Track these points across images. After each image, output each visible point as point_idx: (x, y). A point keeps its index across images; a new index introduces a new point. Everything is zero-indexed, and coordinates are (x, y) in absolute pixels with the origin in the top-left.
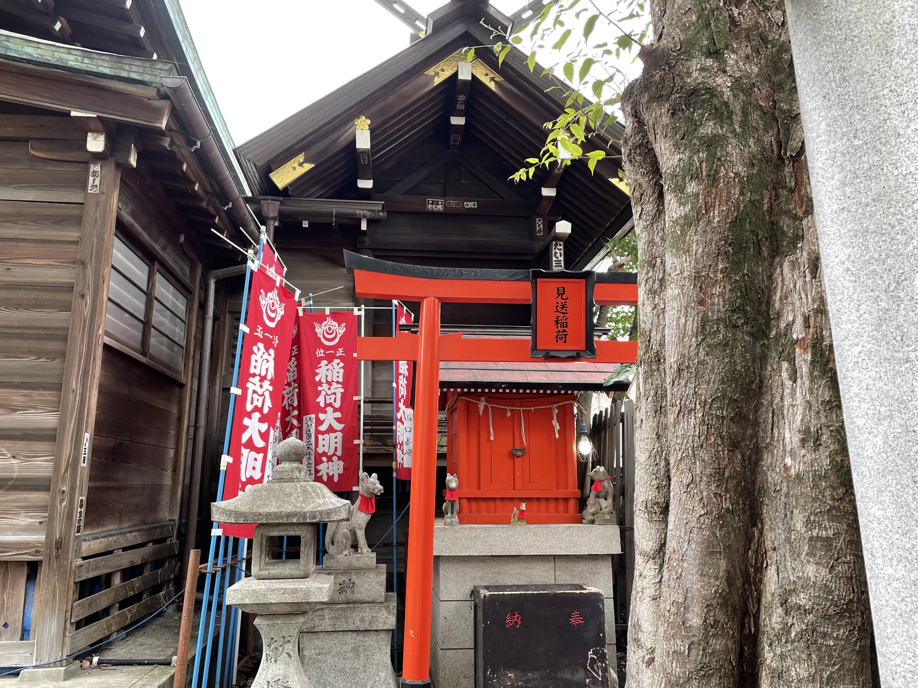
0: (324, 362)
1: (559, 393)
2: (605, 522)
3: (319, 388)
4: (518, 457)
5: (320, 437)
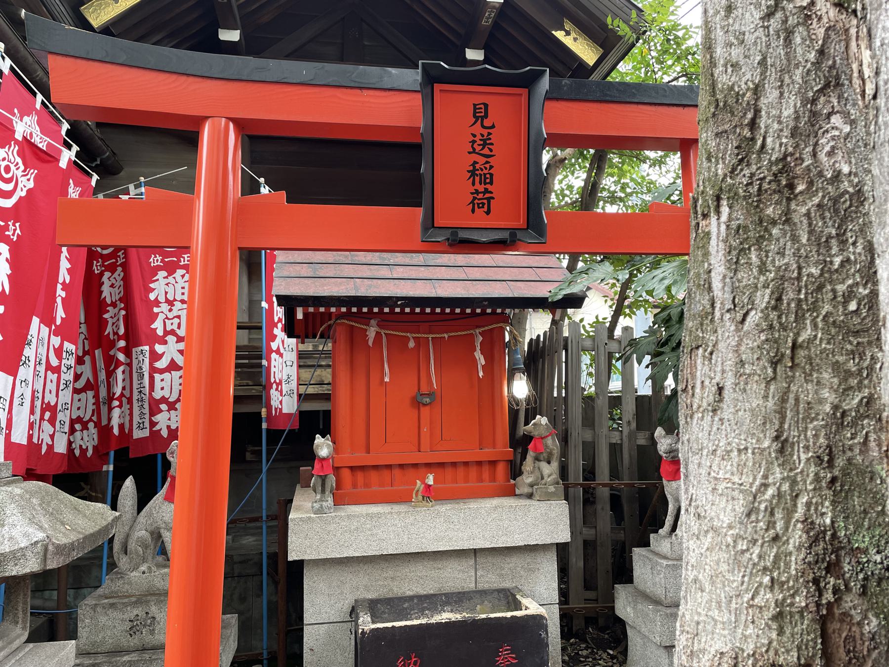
0: (162, 274)
1: (484, 313)
2: (548, 497)
3: (156, 310)
4: (424, 405)
5: (157, 377)
